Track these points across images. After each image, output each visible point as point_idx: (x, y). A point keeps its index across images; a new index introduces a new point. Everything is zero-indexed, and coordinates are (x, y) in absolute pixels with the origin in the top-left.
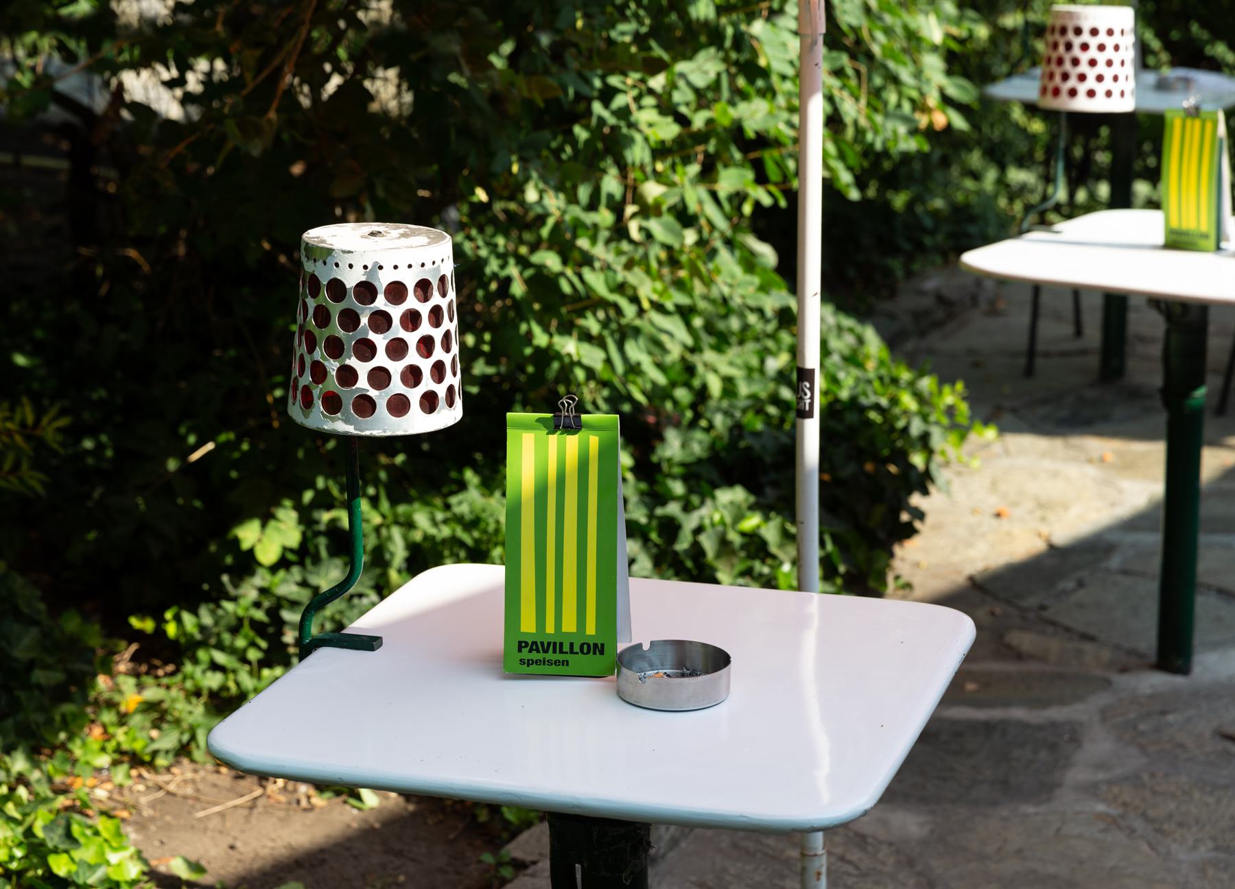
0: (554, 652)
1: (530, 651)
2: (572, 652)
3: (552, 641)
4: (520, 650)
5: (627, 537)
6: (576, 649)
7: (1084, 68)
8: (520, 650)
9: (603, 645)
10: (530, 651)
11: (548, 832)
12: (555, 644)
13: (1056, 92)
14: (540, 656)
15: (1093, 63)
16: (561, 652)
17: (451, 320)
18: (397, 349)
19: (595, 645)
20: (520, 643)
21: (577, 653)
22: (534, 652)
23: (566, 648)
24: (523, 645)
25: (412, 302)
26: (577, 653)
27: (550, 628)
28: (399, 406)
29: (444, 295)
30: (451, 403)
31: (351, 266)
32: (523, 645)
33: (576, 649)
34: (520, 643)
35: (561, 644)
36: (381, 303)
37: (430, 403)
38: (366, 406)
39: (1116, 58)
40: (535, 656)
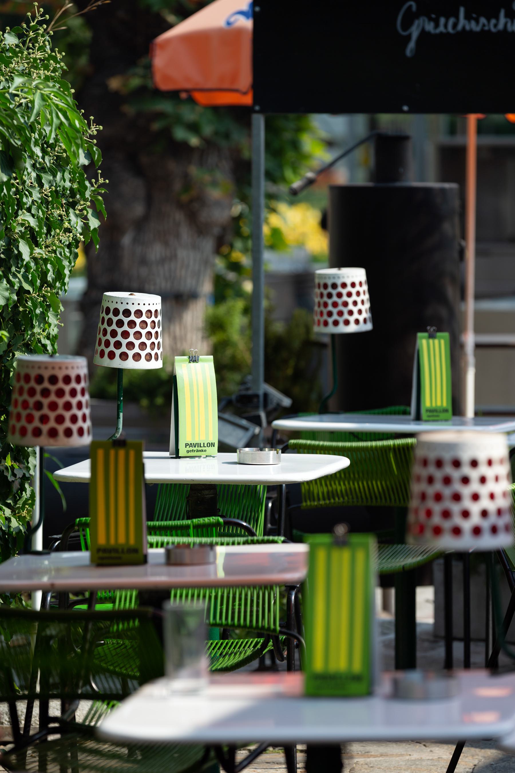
0: (198, 447)
1: (189, 447)
2: (204, 447)
3: (197, 443)
4: (186, 447)
5: (218, 452)
6: (206, 445)
7: (351, 307)
8: (186, 447)
9: (214, 443)
10: (189, 447)
11: (325, 117)
12: (198, 443)
13: (326, 324)
14: (191, 449)
15: (355, 303)
16: (200, 447)
17: (159, 328)
18: (138, 335)
19: (212, 443)
20: (186, 444)
21: (206, 447)
22: (191, 447)
23: (202, 445)
24: (187, 445)
25: (144, 318)
26: (206, 447)
27: (112, 541)
28: (137, 357)
29: (156, 317)
30: (157, 359)
31: (122, 303)
32: (187, 445)
33: (206, 445)
34: (186, 444)
35: (200, 444)
36: (133, 317)
37: (149, 357)
38: (457, 531)
39: (359, 300)
40: (191, 449)
